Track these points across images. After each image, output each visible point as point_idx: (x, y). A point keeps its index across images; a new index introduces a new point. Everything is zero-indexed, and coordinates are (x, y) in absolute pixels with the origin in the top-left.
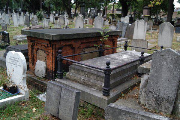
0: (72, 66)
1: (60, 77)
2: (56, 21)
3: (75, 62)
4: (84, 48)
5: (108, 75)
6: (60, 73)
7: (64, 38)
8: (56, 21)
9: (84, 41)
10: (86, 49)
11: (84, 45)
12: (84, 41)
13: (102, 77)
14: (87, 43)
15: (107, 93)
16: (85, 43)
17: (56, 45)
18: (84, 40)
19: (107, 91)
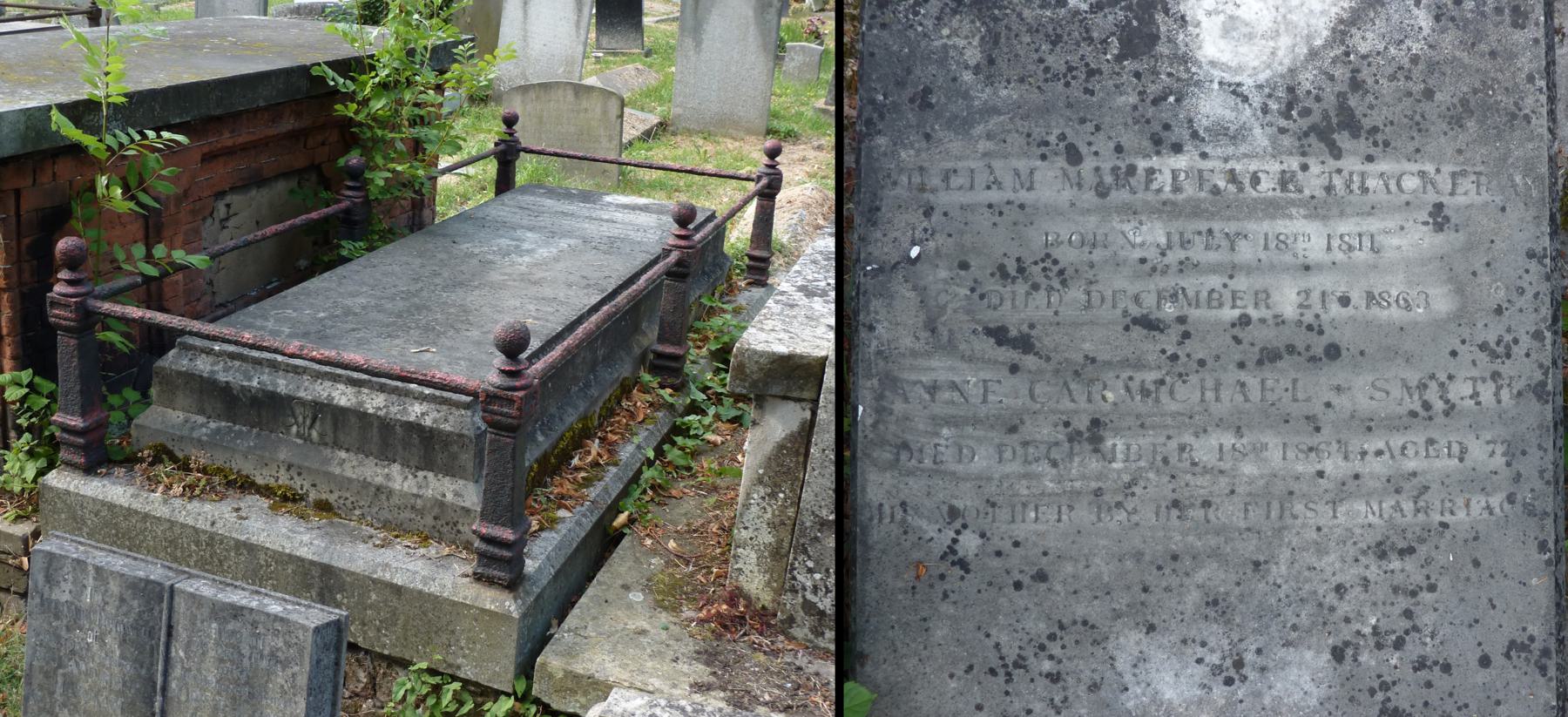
0: (172, 360)
1: (80, 460)
2: (980, 137)
3: (191, 333)
4: (220, 195)
5: (512, 429)
6: (76, 422)
7: (846, 470)
8: (980, 137)
9: (227, 139)
10: (235, 199)
11: (222, 172)
12: (227, 139)
13: (827, 651)
14: (244, 148)
15: (508, 561)
16: (229, 152)
17: (18, 193)
18: (227, 135)
19: (506, 554)
